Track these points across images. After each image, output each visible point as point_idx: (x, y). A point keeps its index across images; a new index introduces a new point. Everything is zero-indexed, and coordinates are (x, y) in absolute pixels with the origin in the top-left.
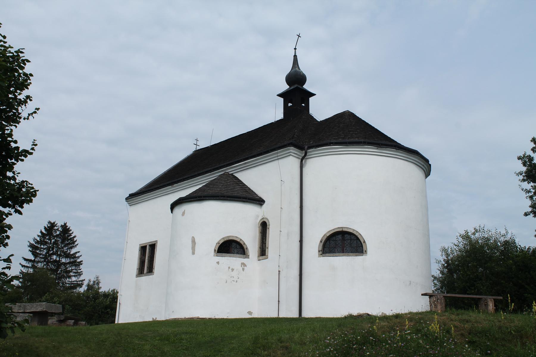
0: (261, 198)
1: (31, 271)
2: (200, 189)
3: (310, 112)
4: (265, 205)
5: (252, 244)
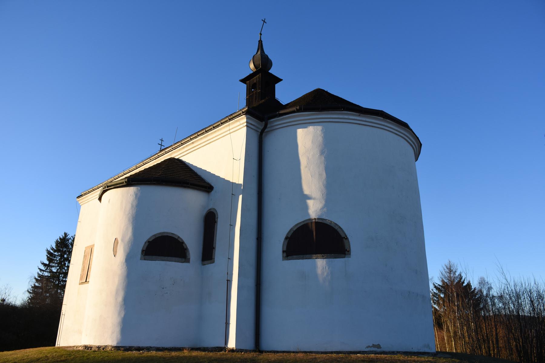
0: (208, 184)
1: (46, 274)
3: (276, 97)
4: (213, 192)
5: (192, 241)
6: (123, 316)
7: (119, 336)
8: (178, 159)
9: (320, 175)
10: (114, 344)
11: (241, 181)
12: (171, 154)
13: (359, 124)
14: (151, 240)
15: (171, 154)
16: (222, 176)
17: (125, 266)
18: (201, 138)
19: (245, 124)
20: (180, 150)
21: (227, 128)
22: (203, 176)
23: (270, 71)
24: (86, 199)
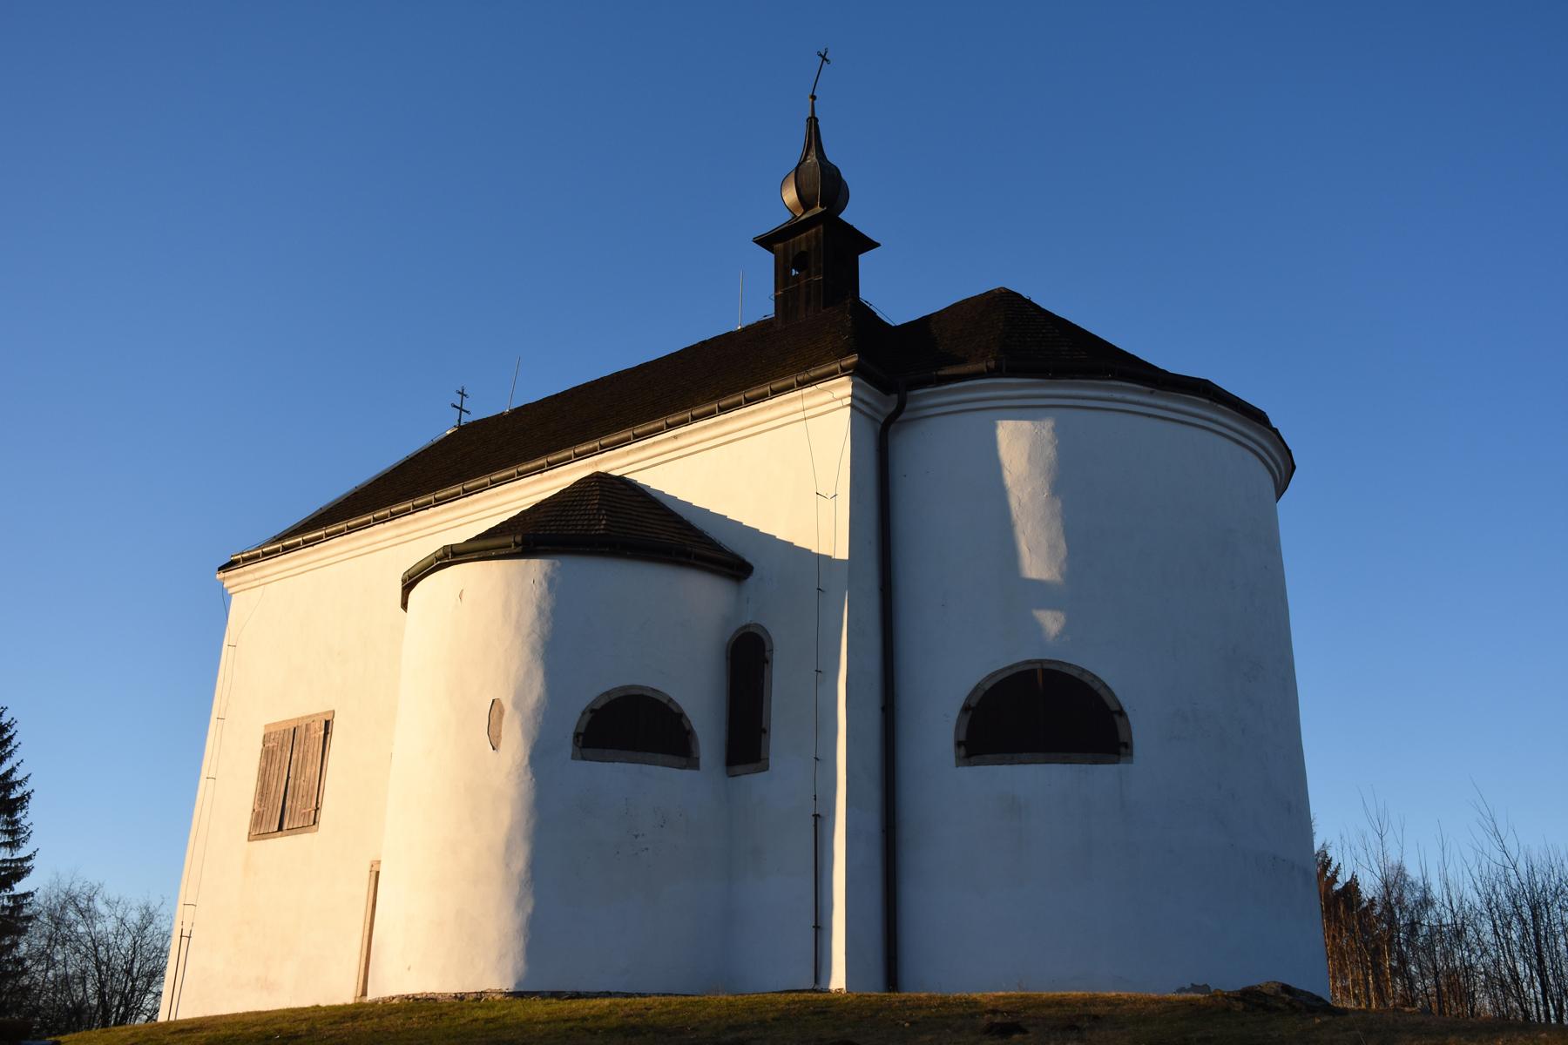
2: (1001, 492)
4: (751, 580)
6: (529, 910)
7: (521, 964)
8: (621, 479)
9: (1052, 547)
10: (509, 986)
11: (842, 552)
12: (596, 463)
13: (1149, 416)
14: (597, 707)
15: (596, 463)
16: (782, 535)
17: (529, 775)
18: (705, 427)
19: (849, 401)
20: (628, 453)
21: (799, 405)
22: (713, 533)
23: (843, 216)
24: (257, 575)
